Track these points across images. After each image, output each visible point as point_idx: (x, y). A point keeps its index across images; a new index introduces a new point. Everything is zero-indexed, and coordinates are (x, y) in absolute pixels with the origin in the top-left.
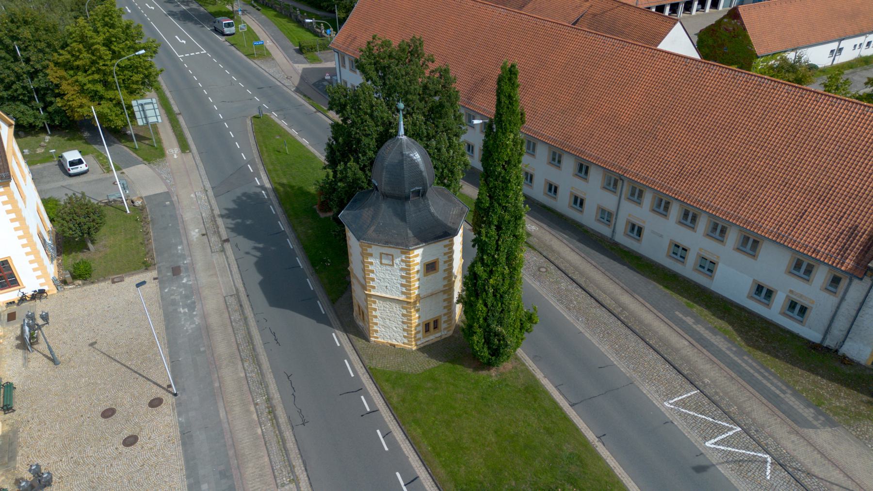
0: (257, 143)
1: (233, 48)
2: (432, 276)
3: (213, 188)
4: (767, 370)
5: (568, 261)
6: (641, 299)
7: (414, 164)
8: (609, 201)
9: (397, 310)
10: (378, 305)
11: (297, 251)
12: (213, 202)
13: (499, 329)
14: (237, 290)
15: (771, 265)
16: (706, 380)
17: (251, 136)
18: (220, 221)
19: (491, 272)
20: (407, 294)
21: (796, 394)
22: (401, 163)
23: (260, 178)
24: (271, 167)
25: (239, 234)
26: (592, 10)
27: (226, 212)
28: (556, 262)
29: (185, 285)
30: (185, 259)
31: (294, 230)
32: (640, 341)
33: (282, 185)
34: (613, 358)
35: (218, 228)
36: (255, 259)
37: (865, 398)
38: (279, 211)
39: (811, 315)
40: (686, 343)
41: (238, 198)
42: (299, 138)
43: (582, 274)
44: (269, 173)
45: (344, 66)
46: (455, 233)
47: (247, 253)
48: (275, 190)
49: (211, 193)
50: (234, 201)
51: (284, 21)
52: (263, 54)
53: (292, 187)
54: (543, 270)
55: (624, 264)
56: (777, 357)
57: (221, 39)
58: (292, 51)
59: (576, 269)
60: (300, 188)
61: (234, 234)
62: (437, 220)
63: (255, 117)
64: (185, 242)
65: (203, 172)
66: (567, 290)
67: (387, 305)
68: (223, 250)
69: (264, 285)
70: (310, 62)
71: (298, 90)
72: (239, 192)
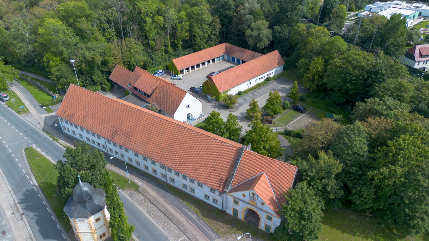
0: (29, 163)
1: (9, 109)
2: (99, 222)
3: (13, 190)
4: (205, 223)
5: (152, 196)
6: (173, 206)
7: (86, 192)
8: (163, 171)
9: (89, 235)
10: (82, 234)
11: (52, 213)
12: (14, 197)
13: (121, 235)
14: (30, 235)
15: (206, 190)
16: (188, 232)
17: (25, 159)
18: (19, 206)
19: (115, 221)
20: (91, 230)
21: (212, 230)
22: (82, 193)
23: (32, 181)
24: (37, 175)
25: (28, 210)
26: (160, 85)
27: (20, 201)
28: (147, 197)
29: (9, 238)
30: (7, 226)
31: (50, 204)
32: (171, 222)
33: (42, 183)
34: (163, 231)
35: (18, 209)
36: (35, 220)
37: (230, 226)
38: (42, 195)
39: (219, 202)
40: (185, 219)
41: (25, 193)
42: (47, 157)
43: (156, 200)
44: (36, 178)
45: (63, 121)
46: (104, 207)
47: (32, 218)
48: (40, 186)
49: (12, 192)
50: (23, 195)
51: (31, 88)
52: (25, 111)
53: (47, 183)
54: (143, 201)
55: (169, 193)
56: (210, 218)
57: (3, 103)
58: (38, 107)
59: (154, 198)
60: (50, 184)
61: (25, 211)
62: (97, 205)
63: (26, 149)
64: (5, 219)
65: (7, 182)
66: (150, 208)
67: (85, 234)
68: (22, 219)
69: (40, 231)
70: (48, 113)
71: (44, 130)
72: (24, 189)
